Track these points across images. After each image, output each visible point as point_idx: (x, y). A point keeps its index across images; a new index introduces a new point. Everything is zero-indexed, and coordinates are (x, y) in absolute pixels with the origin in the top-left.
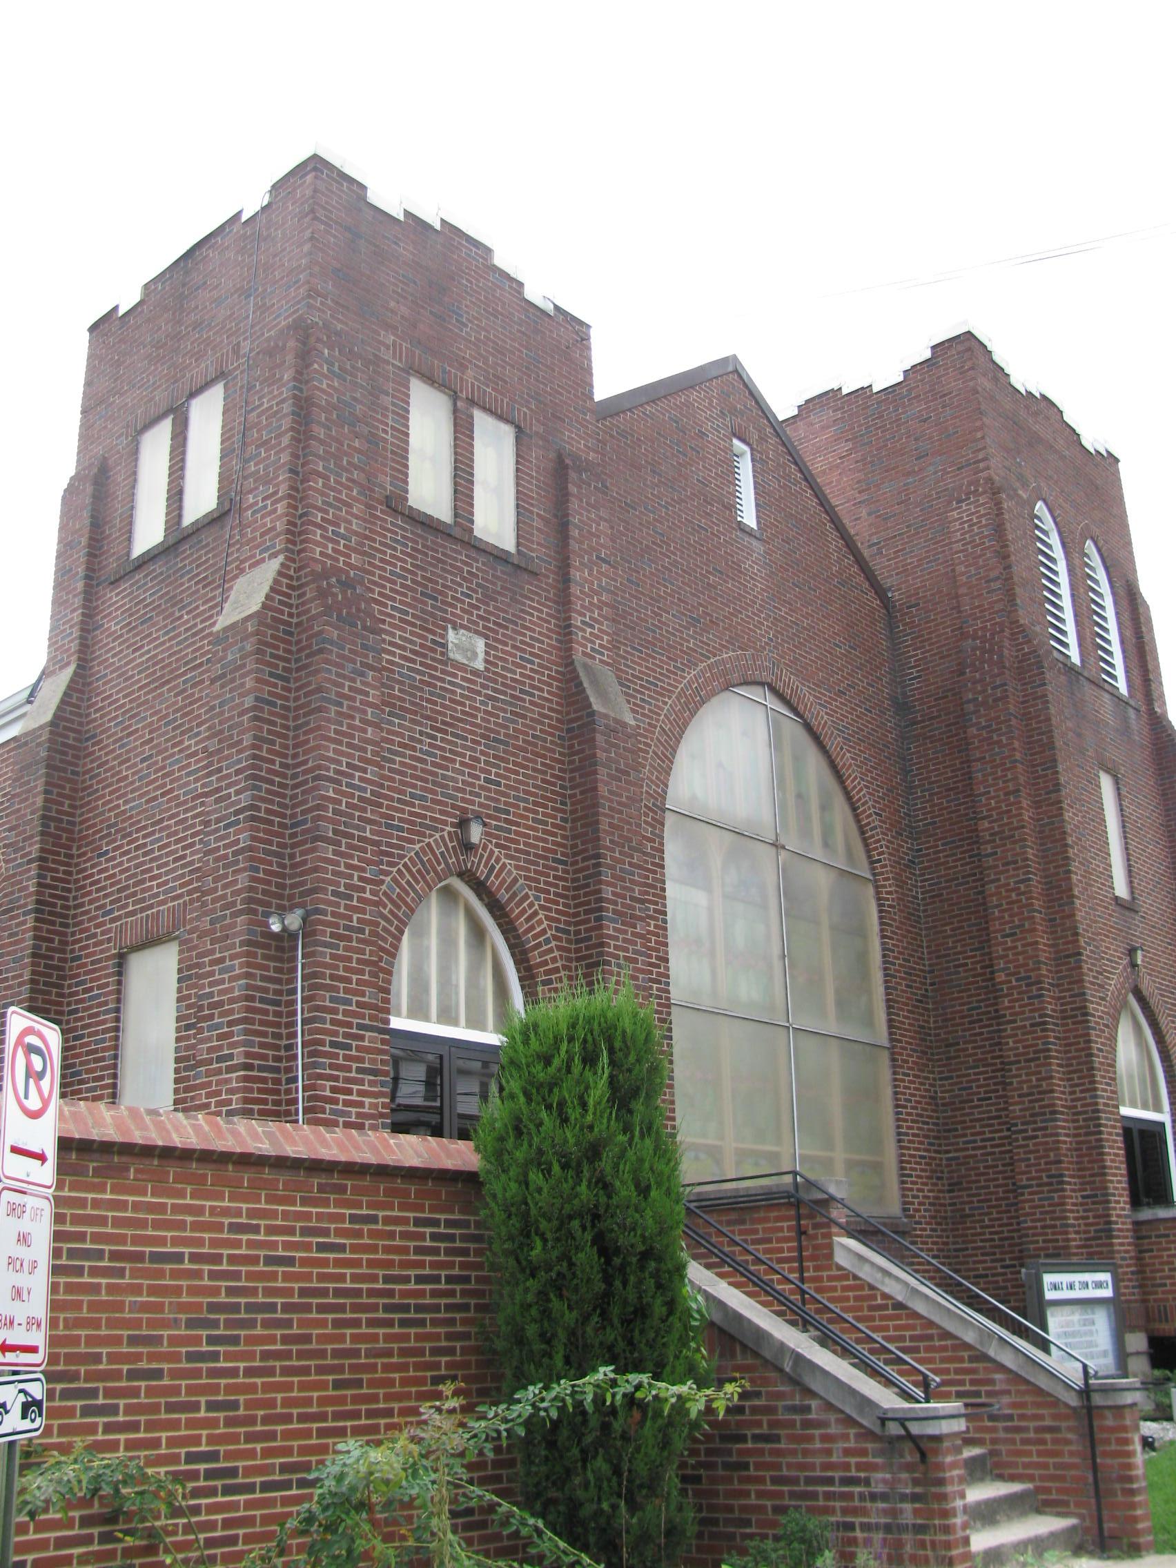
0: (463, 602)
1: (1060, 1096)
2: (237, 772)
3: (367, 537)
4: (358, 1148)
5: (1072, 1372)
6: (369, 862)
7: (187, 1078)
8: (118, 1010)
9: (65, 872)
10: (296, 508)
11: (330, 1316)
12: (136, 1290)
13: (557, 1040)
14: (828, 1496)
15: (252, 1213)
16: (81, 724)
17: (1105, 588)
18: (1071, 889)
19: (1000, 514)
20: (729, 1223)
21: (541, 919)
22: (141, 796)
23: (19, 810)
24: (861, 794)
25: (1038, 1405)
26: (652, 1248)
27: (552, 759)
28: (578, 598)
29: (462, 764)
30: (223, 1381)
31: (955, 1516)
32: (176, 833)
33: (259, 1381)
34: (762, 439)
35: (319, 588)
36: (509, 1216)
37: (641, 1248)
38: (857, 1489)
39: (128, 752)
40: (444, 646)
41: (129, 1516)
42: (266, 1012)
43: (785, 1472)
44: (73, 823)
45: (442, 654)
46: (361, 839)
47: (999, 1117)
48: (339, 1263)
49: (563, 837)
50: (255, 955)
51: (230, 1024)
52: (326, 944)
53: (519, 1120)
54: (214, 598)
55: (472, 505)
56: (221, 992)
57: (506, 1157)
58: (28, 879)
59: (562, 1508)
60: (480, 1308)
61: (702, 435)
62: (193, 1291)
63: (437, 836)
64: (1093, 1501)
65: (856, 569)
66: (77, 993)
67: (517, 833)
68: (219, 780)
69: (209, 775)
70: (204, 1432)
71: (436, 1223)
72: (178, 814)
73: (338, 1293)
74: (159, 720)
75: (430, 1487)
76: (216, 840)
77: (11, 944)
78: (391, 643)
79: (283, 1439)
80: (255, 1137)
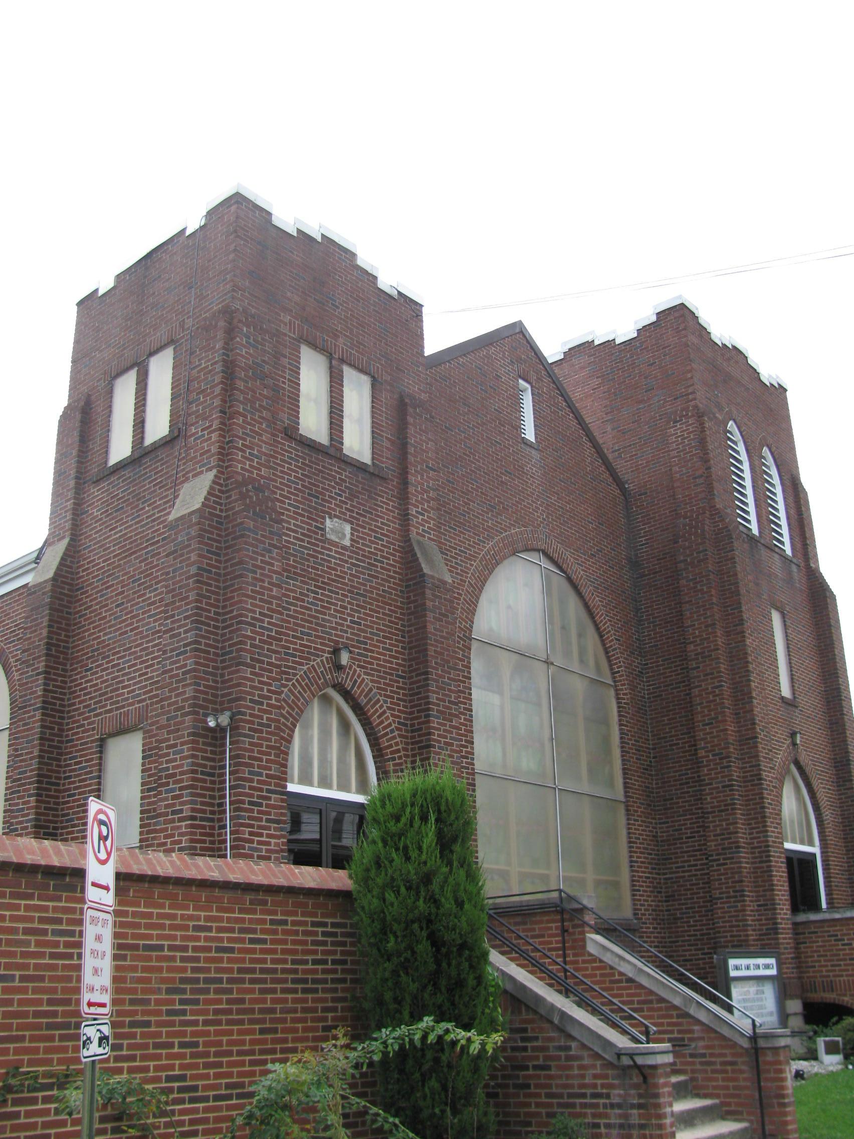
0: (336, 499)
1: (742, 838)
2: (186, 618)
3: (272, 456)
4: (275, 876)
5: (745, 1025)
6: (274, 679)
7: (149, 825)
8: (99, 777)
9: (62, 681)
10: (224, 437)
11: (257, 986)
12: (134, 969)
13: (404, 805)
14: (584, 1106)
15: (207, 919)
16: (73, 579)
17: (776, 480)
18: (750, 693)
19: (703, 431)
20: (516, 924)
21: (388, 718)
22: (115, 631)
23: (30, 638)
24: (606, 626)
25: (722, 1047)
26: (466, 942)
27: (396, 606)
28: (413, 495)
29: (335, 610)
30: (189, 1029)
31: (665, 1118)
32: (141, 657)
33: (212, 1028)
34: (539, 379)
35: (241, 493)
36: (373, 921)
37: (459, 941)
38: (602, 1101)
39: (106, 600)
40: (323, 530)
41: (131, 1117)
42: (205, 781)
43: (554, 1090)
44: (68, 648)
45: (322, 535)
46: (269, 664)
47: (701, 850)
48: (262, 951)
49: (403, 660)
50: (197, 742)
51: (181, 789)
52: (246, 736)
53: (378, 857)
54: (167, 496)
55: (342, 432)
56: (174, 767)
57: (370, 882)
58: (37, 686)
59: (408, 1113)
60: (354, 981)
61: (498, 377)
62: (170, 969)
63: (319, 660)
64: (759, 1111)
65: (603, 468)
66: (70, 765)
67: (372, 657)
68: (173, 622)
69: (166, 618)
70: (177, 1062)
71: (325, 925)
72: (142, 644)
73: (262, 971)
74: (129, 578)
75: (330, 1099)
76: (171, 664)
77: (24, 731)
78: (288, 529)
79: (227, 1067)
80: (210, 868)
